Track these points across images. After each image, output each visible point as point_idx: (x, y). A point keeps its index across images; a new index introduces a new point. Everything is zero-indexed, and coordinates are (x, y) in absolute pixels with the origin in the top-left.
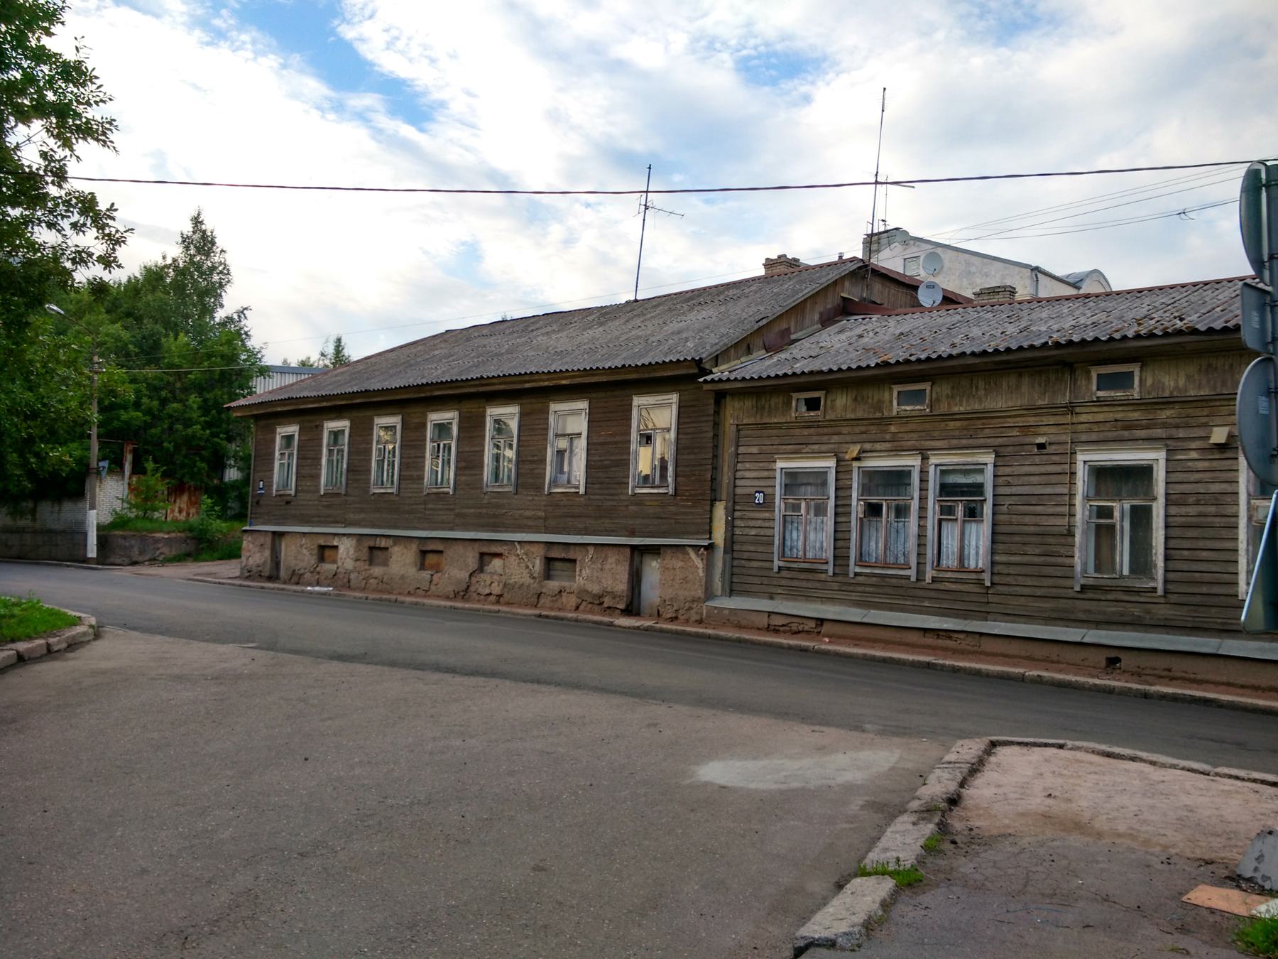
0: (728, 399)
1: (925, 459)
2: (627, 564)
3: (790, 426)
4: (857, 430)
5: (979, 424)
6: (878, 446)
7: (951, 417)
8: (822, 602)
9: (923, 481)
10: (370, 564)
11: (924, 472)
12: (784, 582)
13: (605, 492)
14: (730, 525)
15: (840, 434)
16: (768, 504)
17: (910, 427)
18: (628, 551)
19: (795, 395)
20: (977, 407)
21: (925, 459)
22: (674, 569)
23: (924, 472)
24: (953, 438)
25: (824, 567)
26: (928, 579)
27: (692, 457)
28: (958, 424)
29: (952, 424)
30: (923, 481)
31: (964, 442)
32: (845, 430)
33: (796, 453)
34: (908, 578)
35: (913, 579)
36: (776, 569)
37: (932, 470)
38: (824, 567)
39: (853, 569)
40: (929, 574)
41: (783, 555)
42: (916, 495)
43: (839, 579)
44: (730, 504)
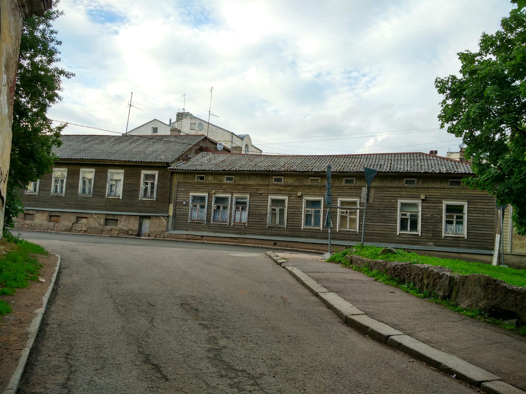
0: (175, 174)
1: (232, 195)
2: (138, 221)
3: (195, 183)
4: (214, 186)
5: (246, 187)
6: (220, 191)
7: (239, 185)
8: (202, 232)
9: (232, 200)
10: (24, 220)
11: (232, 198)
12: (191, 226)
13: (130, 199)
14: (175, 210)
15: (209, 187)
16: (187, 204)
17: (229, 186)
18: (139, 217)
19: (197, 175)
20: (246, 183)
21: (232, 195)
22: (156, 223)
23: (232, 198)
24: (240, 190)
25: (204, 222)
26: (232, 225)
27: (162, 190)
28: (241, 187)
29: (239, 187)
30: (232, 200)
31: (242, 191)
32: (211, 186)
33: (196, 191)
34: (227, 225)
35: (228, 225)
36: (189, 223)
37: (234, 198)
38: (204, 222)
39: (212, 222)
40: (232, 224)
41: (191, 219)
42: (230, 204)
43: (208, 225)
44: (175, 204)
